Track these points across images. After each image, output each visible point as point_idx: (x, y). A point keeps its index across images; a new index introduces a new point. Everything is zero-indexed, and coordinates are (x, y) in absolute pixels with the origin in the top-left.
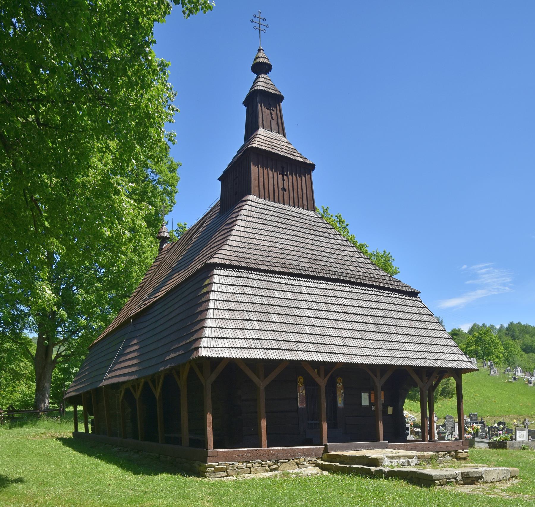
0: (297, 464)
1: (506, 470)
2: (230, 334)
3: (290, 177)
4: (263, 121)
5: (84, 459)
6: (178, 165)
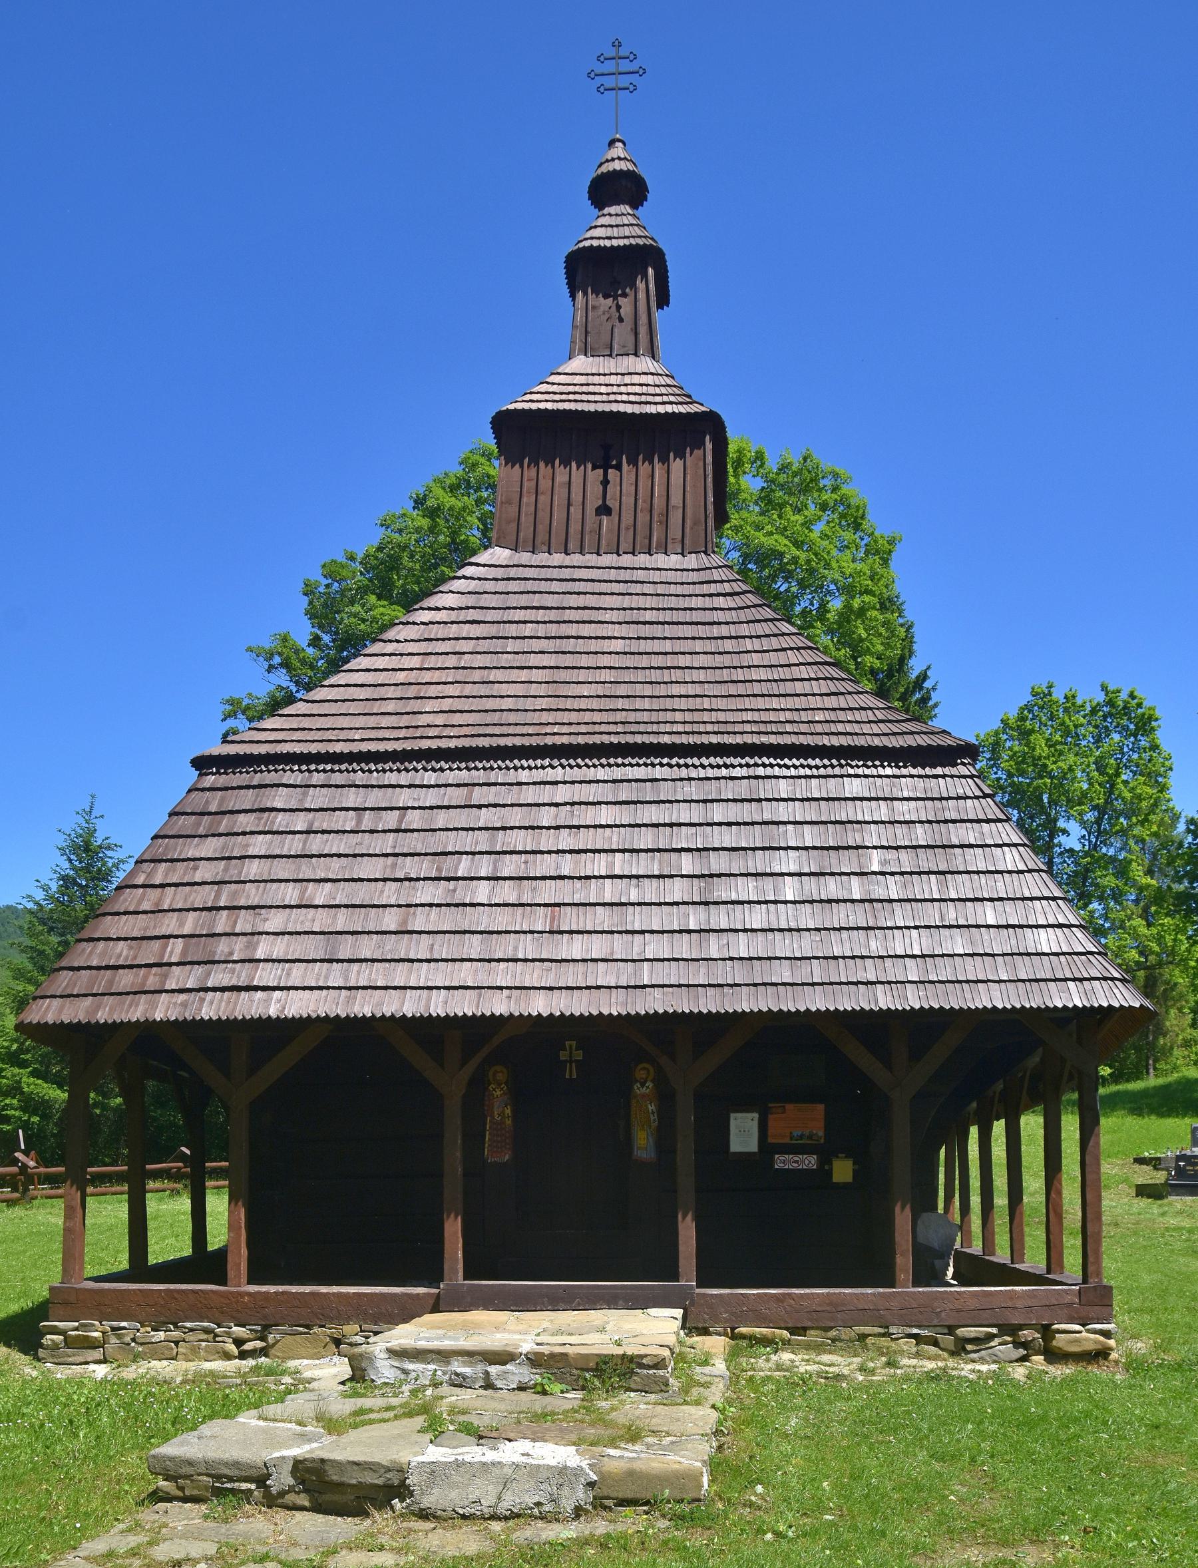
6: (891, 542)
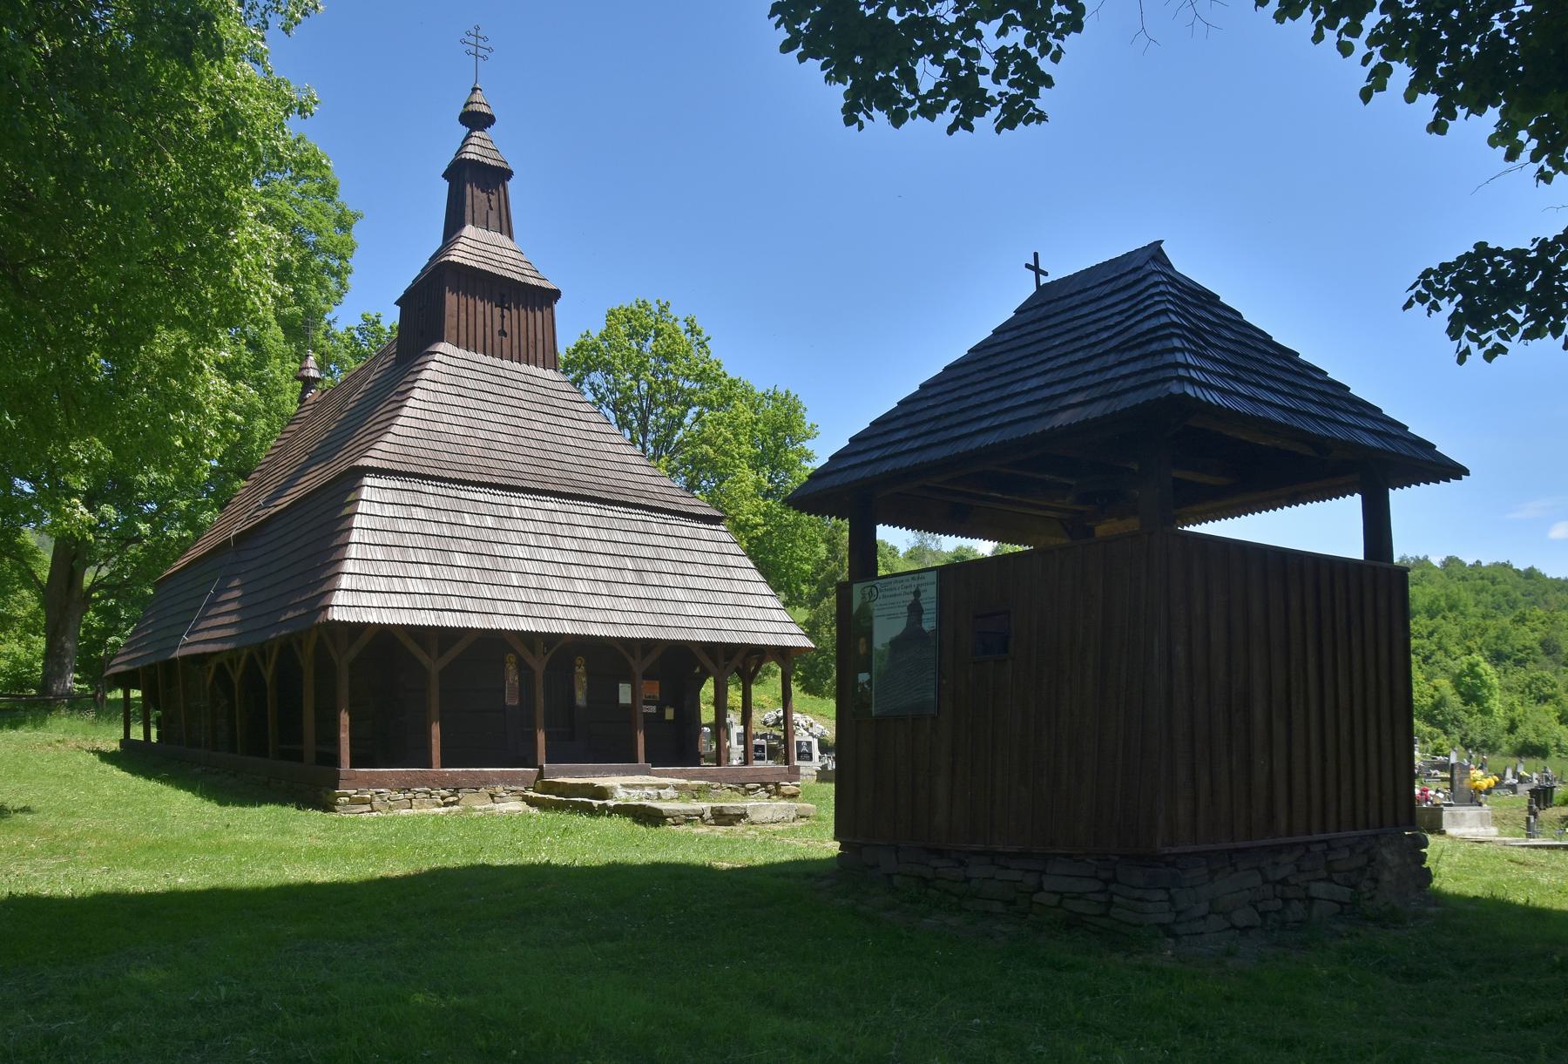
0: (492, 796)
2: (382, 584)
5: (140, 782)
6: (356, 217)
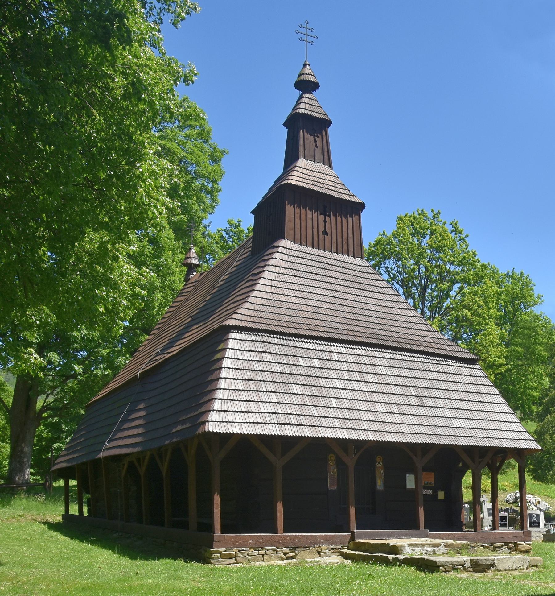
0: (319, 553)
1: (524, 559)
2: (243, 407)
3: (333, 218)
4: (304, 149)
6: (223, 153)
